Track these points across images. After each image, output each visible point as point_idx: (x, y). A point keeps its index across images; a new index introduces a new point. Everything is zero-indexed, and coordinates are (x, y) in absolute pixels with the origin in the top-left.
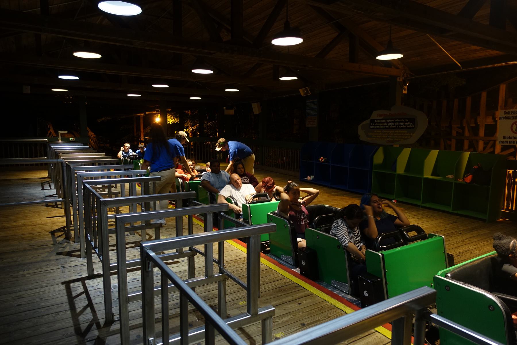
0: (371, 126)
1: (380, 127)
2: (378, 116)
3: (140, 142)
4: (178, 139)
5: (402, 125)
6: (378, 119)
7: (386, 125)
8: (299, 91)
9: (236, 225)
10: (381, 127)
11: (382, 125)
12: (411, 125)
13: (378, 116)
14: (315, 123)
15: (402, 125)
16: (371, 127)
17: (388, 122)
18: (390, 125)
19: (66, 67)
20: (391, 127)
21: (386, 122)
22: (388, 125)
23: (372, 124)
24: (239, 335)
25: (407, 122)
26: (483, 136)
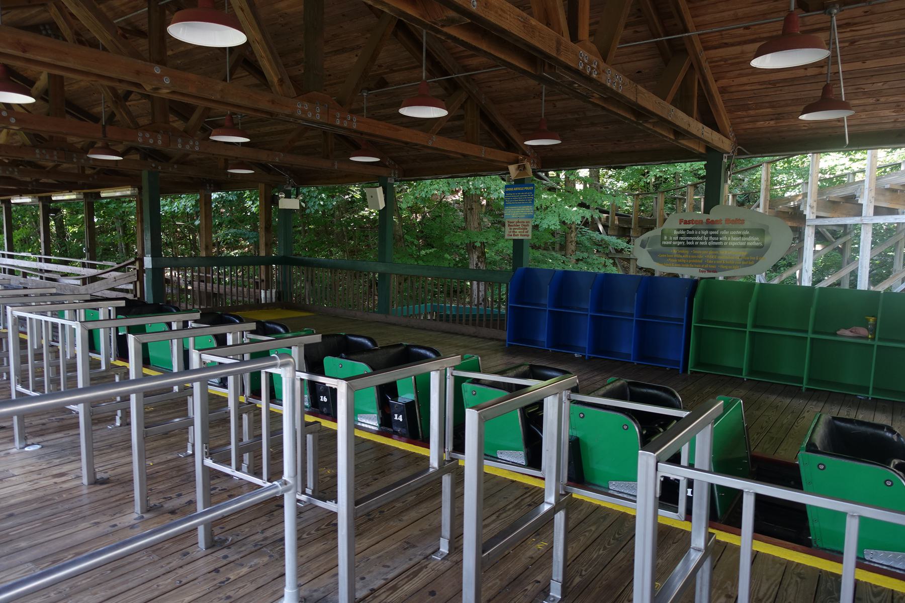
0: (665, 241)
1: (686, 243)
2: (680, 224)
3: (145, 304)
4: (221, 400)
5: (735, 241)
6: (681, 229)
7: (699, 241)
8: (187, 400)
9: (427, 33)
10: (688, 243)
11: (689, 241)
12: (756, 241)
13: (680, 224)
14: (527, 232)
15: (735, 241)
16: (664, 243)
17: (703, 235)
18: (708, 241)
19: (79, 115)
20: (710, 244)
21: (700, 236)
22: (703, 241)
23: (665, 238)
24: (268, 309)
25: (747, 236)
26: (228, 377)
